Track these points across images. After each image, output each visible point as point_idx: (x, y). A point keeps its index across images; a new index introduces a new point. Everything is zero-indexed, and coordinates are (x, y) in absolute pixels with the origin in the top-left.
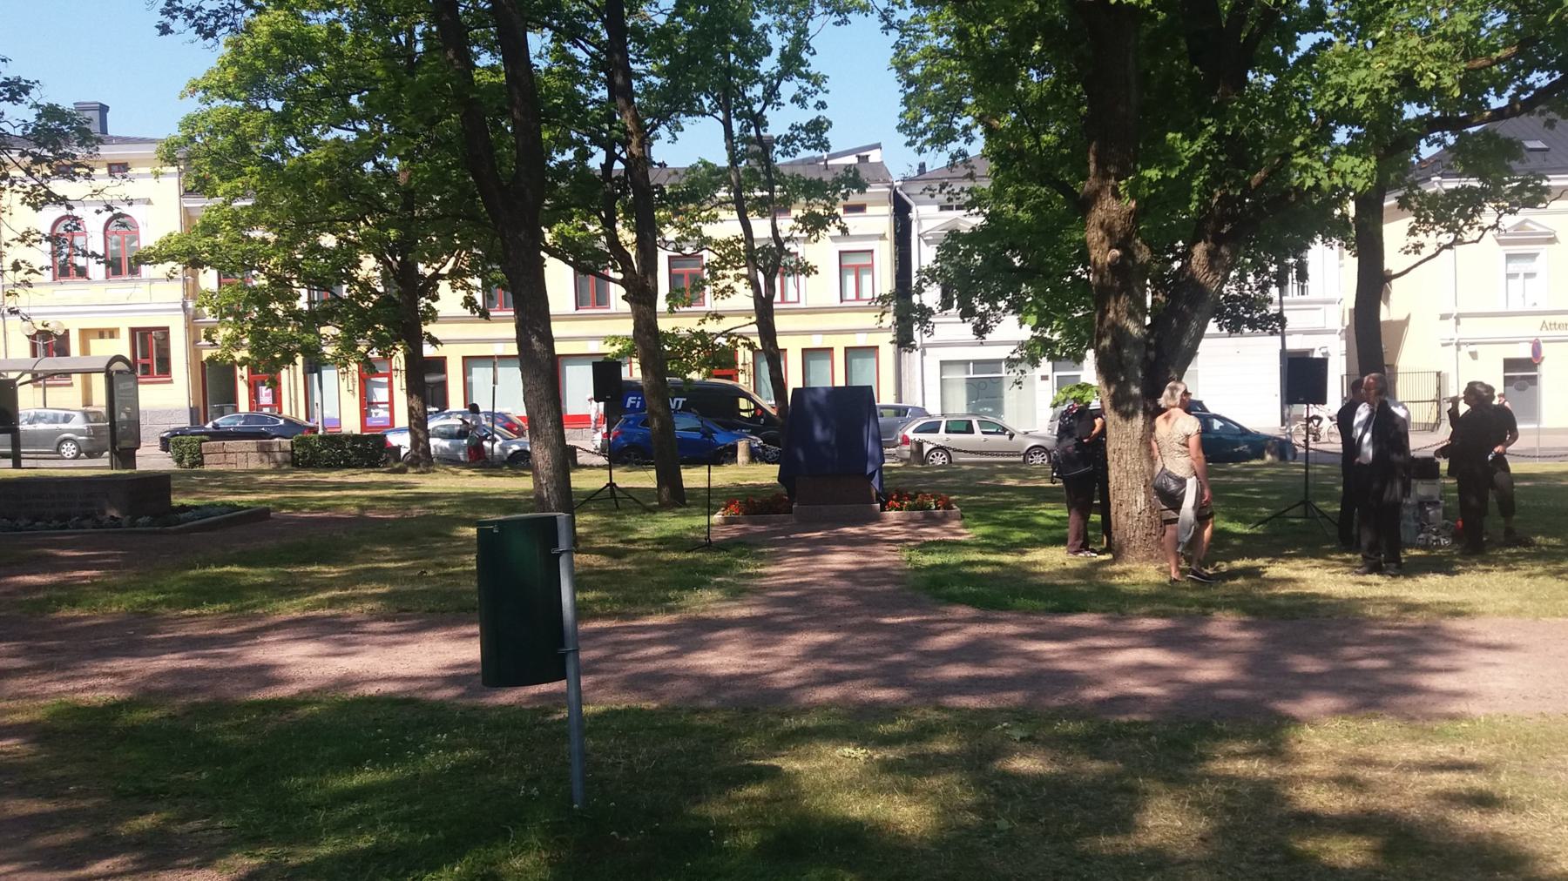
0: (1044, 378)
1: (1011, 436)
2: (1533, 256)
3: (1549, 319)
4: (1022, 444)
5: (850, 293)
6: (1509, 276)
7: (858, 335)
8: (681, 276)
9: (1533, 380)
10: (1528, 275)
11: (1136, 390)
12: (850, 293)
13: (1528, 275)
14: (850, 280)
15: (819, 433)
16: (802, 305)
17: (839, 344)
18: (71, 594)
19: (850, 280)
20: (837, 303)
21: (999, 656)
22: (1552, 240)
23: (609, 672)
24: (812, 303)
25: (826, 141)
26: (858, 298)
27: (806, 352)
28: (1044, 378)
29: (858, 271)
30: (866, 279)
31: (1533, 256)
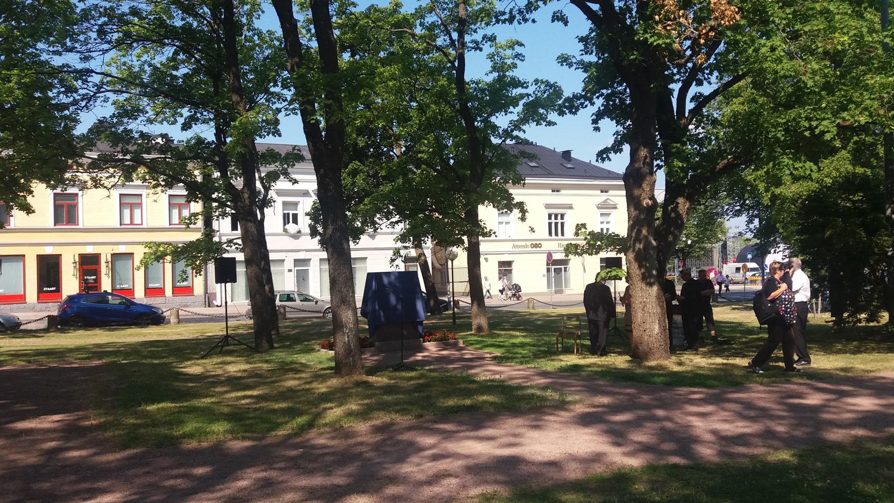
0: (290, 271)
1: (316, 302)
2: (609, 214)
3: (516, 243)
4: (322, 307)
5: (127, 220)
6: (500, 223)
7: (87, 247)
8: (62, 206)
9: (510, 271)
10: (507, 223)
11: (654, 272)
12: (127, 220)
13: (507, 223)
14: (127, 212)
15: (393, 299)
16: (144, 226)
17: (105, 253)
18: (364, 414)
19: (127, 212)
20: (118, 226)
21: (62, 430)
22: (615, 208)
23: (834, 413)
24: (88, 225)
25: (279, 130)
26: (132, 223)
27: (114, 256)
28: (290, 271)
29: (132, 206)
30: (137, 212)
31: (609, 214)
